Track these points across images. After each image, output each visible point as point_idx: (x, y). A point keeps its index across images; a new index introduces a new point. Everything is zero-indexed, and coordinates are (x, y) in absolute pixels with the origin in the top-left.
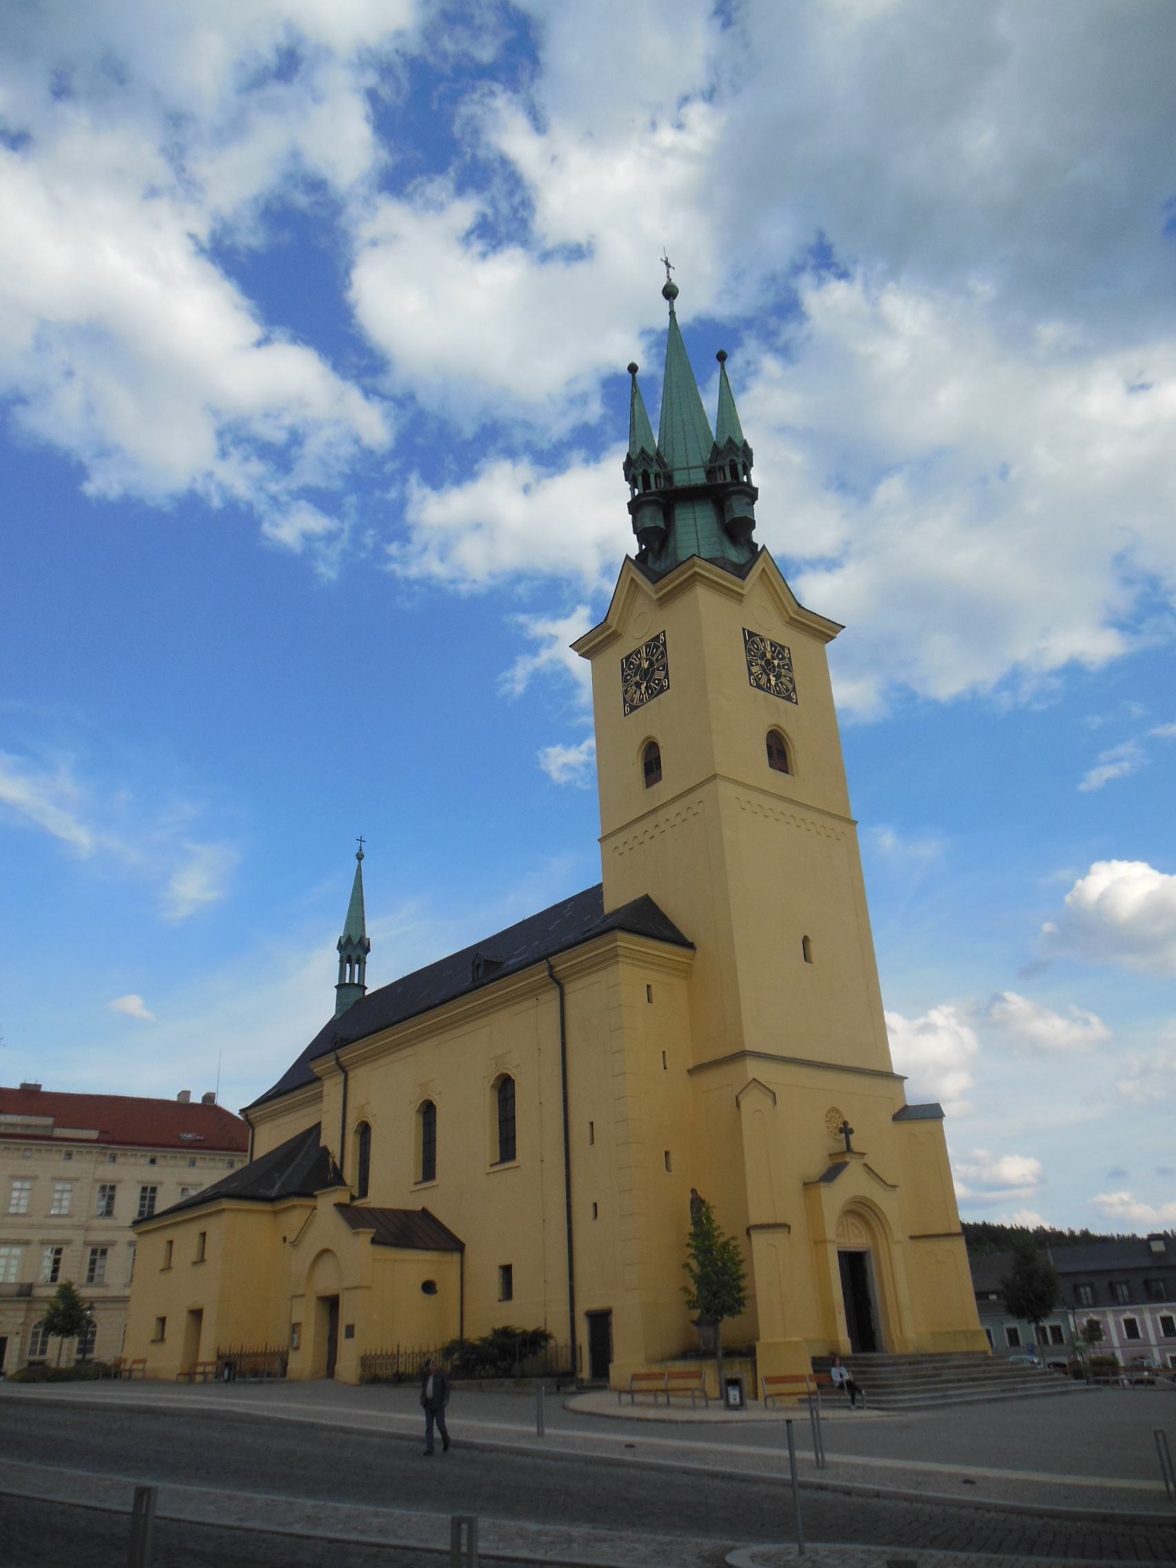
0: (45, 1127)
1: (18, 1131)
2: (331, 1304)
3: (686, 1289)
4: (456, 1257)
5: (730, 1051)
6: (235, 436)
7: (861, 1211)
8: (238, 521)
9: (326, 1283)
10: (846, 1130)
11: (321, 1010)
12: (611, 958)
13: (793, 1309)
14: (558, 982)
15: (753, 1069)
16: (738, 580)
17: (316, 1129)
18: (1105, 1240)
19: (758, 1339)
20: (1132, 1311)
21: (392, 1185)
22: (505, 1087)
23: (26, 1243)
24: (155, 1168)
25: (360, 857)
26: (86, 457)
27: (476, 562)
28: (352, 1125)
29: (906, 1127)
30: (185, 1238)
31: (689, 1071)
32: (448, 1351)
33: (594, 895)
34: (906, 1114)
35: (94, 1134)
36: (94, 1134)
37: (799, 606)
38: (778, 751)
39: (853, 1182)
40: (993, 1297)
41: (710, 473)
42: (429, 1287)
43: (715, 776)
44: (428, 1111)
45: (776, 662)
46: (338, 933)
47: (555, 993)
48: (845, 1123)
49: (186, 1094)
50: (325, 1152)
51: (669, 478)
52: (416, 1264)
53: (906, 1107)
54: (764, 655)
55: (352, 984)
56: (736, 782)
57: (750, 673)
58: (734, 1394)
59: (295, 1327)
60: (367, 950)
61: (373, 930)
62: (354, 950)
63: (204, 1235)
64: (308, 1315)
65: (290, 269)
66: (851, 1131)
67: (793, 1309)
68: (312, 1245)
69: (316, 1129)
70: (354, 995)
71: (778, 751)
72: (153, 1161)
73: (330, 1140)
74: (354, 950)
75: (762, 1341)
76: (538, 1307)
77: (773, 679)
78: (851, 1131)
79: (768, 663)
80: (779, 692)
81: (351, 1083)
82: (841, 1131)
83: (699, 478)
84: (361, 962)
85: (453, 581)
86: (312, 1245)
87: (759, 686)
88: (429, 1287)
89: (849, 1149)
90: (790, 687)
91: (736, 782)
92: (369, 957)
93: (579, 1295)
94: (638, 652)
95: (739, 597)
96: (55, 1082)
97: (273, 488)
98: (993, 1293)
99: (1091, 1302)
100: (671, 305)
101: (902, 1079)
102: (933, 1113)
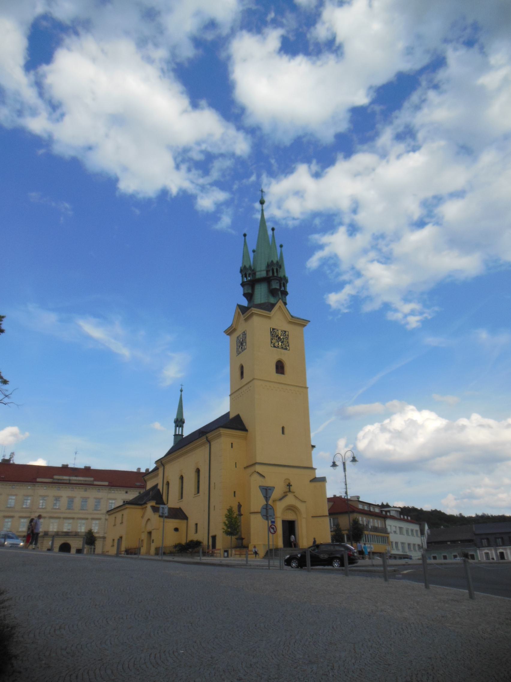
0: (91, 481)
1: (83, 482)
2: (150, 533)
3: (223, 529)
4: (185, 521)
5: (254, 462)
6: (183, 158)
7: (291, 508)
8: (186, 200)
9: (149, 528)
10: (289, 485)
11: (170, 444)
12: (219, 436)
13: (260, 534)
14: (209, 442)
15: (258, 468)
16: (268, 312)
17: (157, 485)
18: (460, 521)
19: (250, 543)
20: (502, 549)
21: (173, 501)
22: (198, 471)
23: (87, 519)
24: (127, 495)
25: (181, 391)
26: (119, 174)
27: (295, 208)
28: (165, 482)
29: (314, 484)
30: (119, 515)
31: (245, 468)
32: (175, 546)
33: (228, 414)
34: (315, 480)
35: (106, 483)
36: (106, 483)
37: (292, 316)
38: (280, 367)
39: (290, 500)
40: (449, 543)
41: (267, 272)
42: (176, 530)
43: (254, 379)
44: (182, 478)
45: (282, 337)
46: (175, 417)
47: (208, 445)
48: (289, 483)
49: (139, 469)
50: (159, 490)
51: (254, 274)
52: (172, 523)
53: (316, 478)
54: (278, 335)
55: (179, 435)
56: (260, 380)
57: (272, 342)
58: (226, 554)
59: (142, 540)
60: (184, 422)
61: (186, 416)
62: (179, 422)
63: (123, 515)
64: (144, 536)
65: (204, 76)
66: (291, 486)
67: (260, 534)
68: (146, 518)
69: (157, 485)
70: (179, 438)
71: (280, 367)
72: (127, 492)
73: (160, 487)
74: (179, 422)
75: (251, 544)
76: (202, 536)
77: (280, 344)
78: (291, 486)
79: (279, 338)
80: (282, 348)
81: (165, 469)
82: (288, 485)
83: (264, 274)
84: (182, 426)
85: (285, 219)
86: (146, 518)
87: (274, 347)
88: (176, 530)
89: (290, 491)
90: (287, 345)
91: (260, 380)
92: (185, 425)
93: (211, 531)
94: (240, 336)
95: (269, 318)
96: (97, 464)
97: (201, 181)
98: (449, 541)
99: (501, 544)
100: (262, 207)
101: (315, 469)
102: (323, 480)
